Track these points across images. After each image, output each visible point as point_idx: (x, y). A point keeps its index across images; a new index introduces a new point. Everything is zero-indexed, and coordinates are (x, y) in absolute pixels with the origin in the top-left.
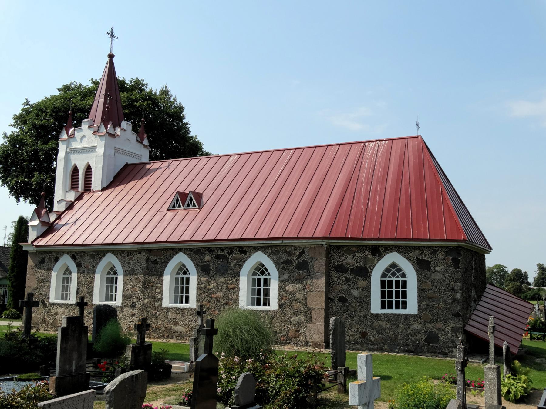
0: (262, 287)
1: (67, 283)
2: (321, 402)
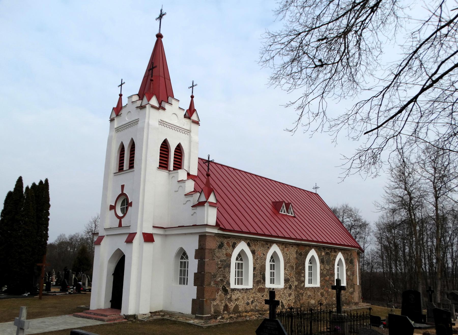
1: (185, 267)
2: (305, 333)
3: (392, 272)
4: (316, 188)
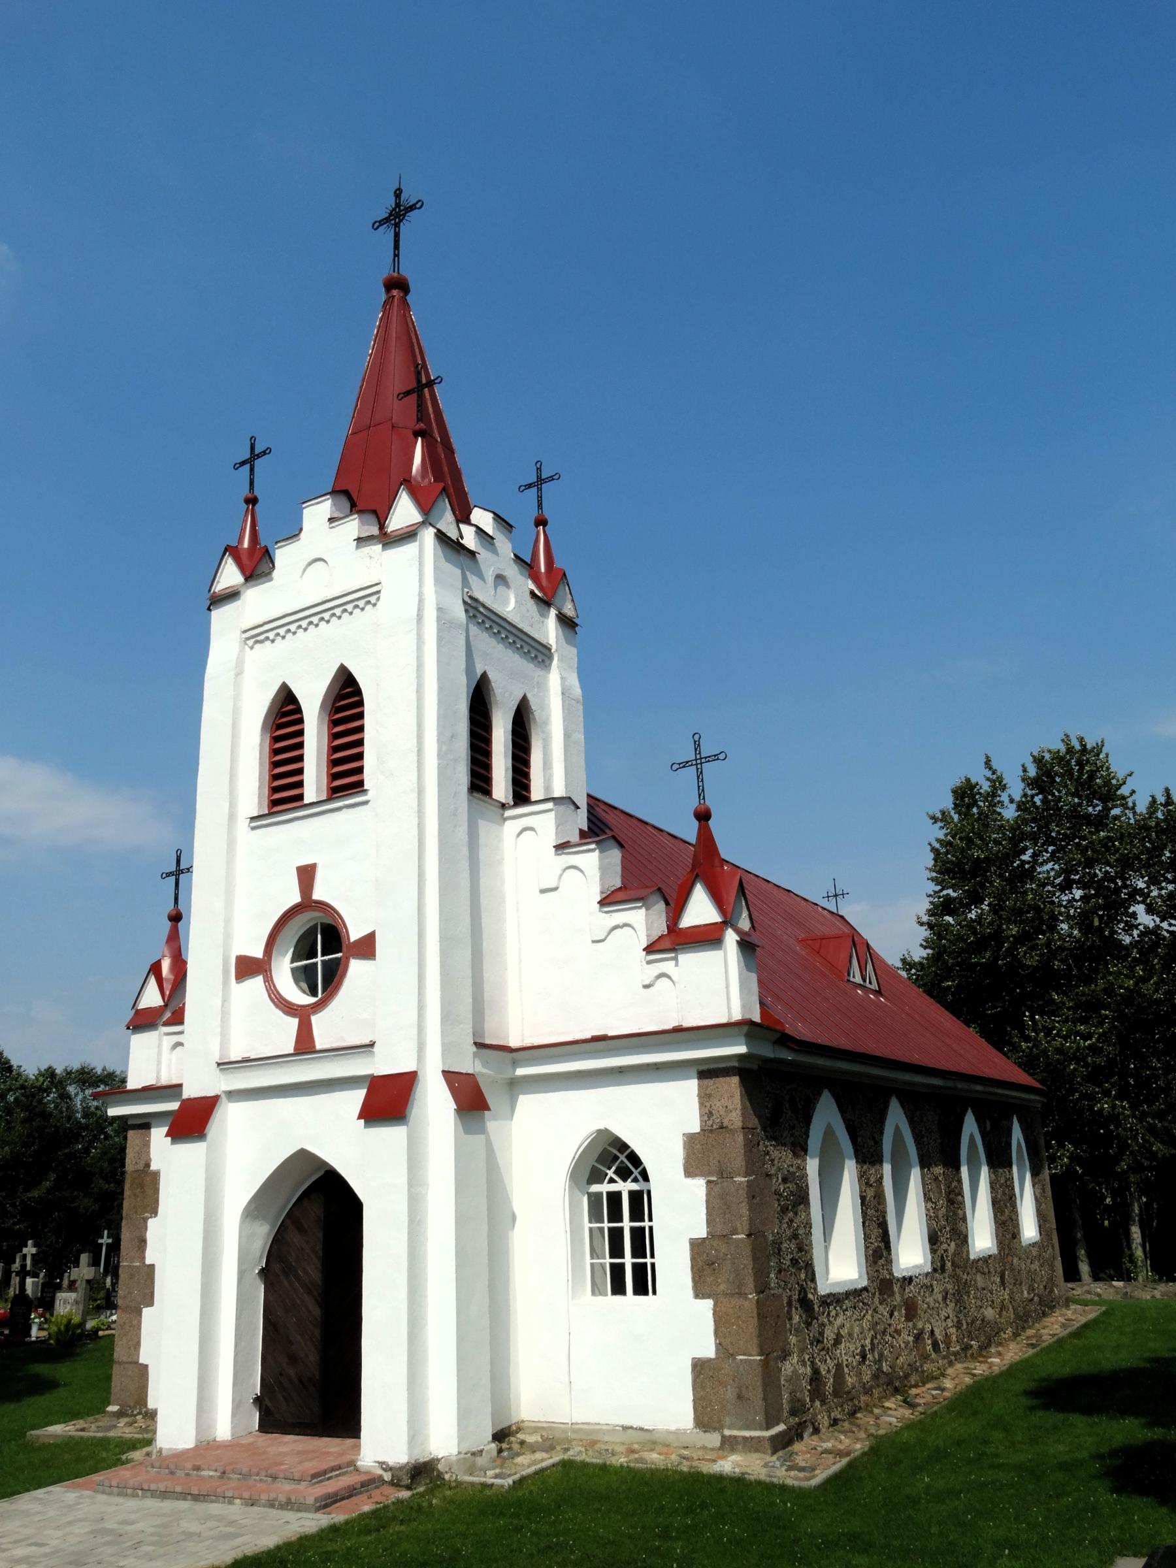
0: (627, 1224)
4: (836, 896)
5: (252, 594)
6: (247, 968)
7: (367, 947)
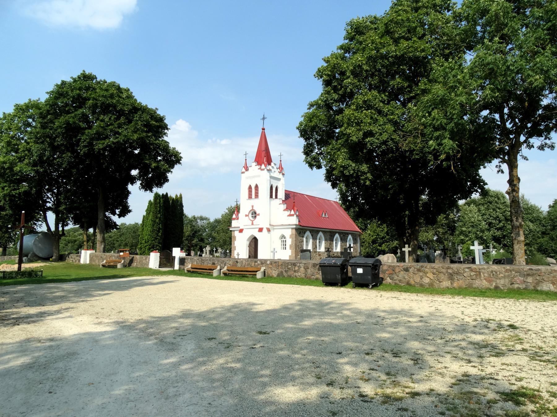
3: (15, 167)
5: (246, 172)
6: (246, 216)
7: (259, 215)
